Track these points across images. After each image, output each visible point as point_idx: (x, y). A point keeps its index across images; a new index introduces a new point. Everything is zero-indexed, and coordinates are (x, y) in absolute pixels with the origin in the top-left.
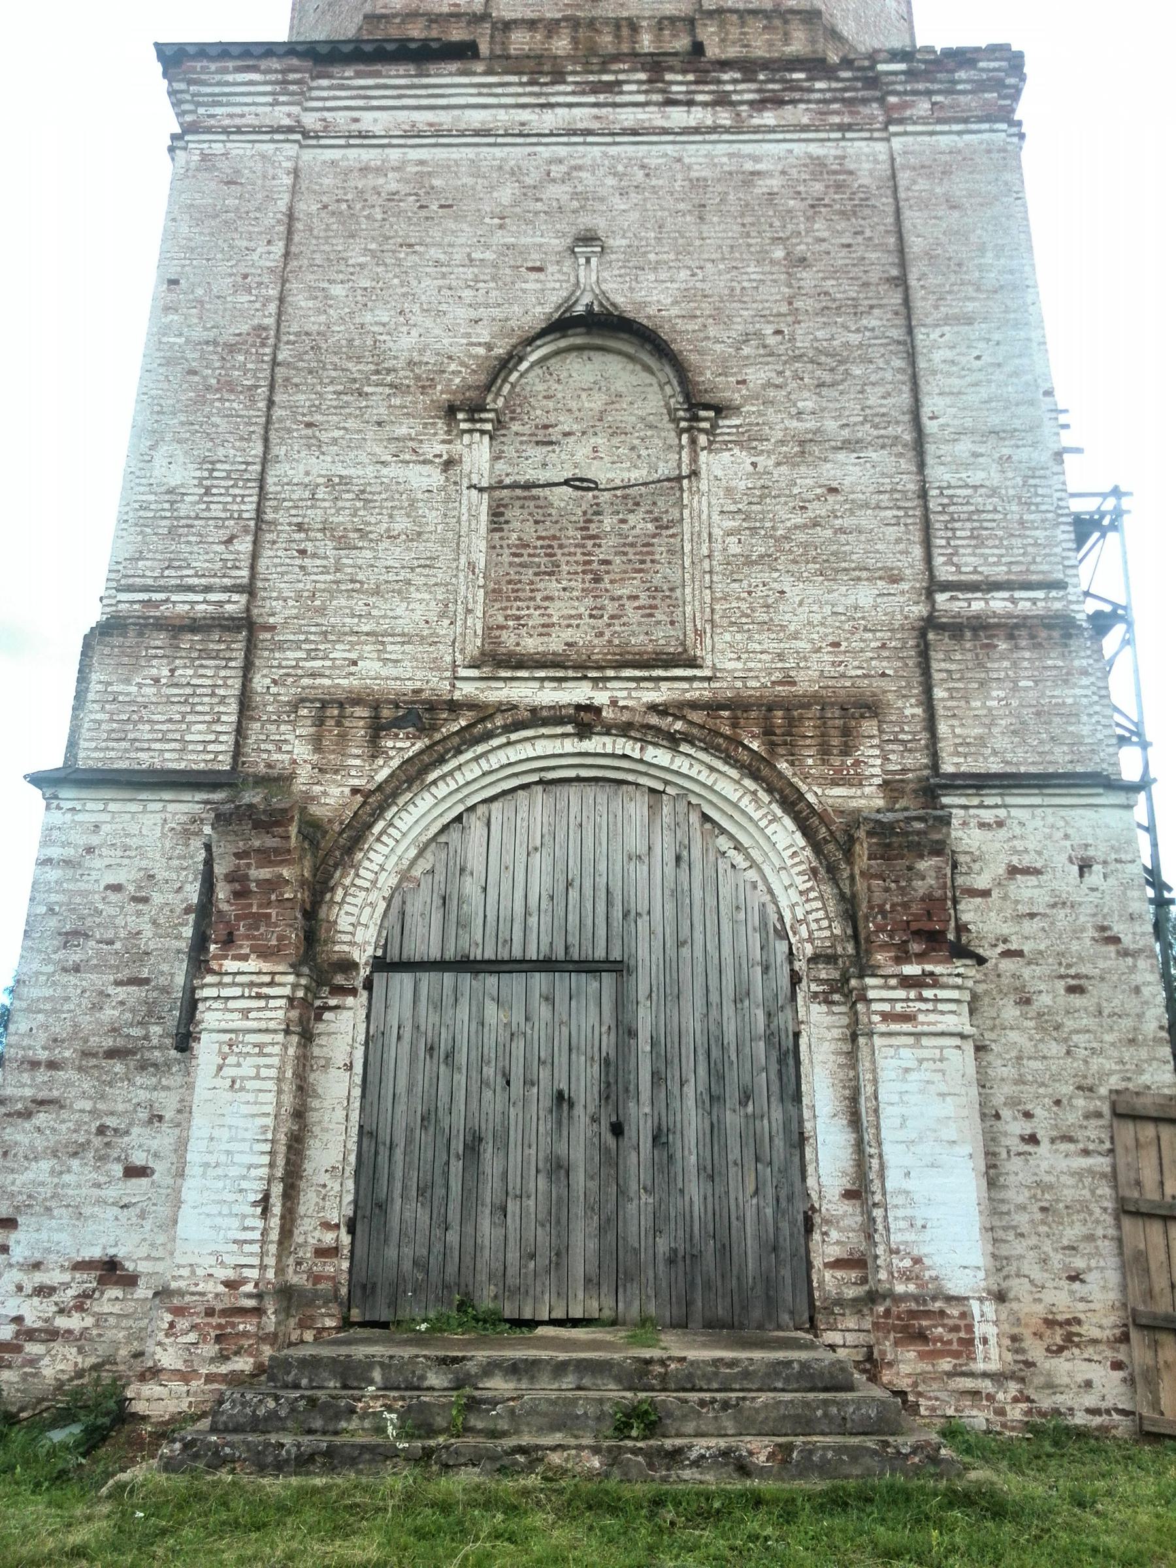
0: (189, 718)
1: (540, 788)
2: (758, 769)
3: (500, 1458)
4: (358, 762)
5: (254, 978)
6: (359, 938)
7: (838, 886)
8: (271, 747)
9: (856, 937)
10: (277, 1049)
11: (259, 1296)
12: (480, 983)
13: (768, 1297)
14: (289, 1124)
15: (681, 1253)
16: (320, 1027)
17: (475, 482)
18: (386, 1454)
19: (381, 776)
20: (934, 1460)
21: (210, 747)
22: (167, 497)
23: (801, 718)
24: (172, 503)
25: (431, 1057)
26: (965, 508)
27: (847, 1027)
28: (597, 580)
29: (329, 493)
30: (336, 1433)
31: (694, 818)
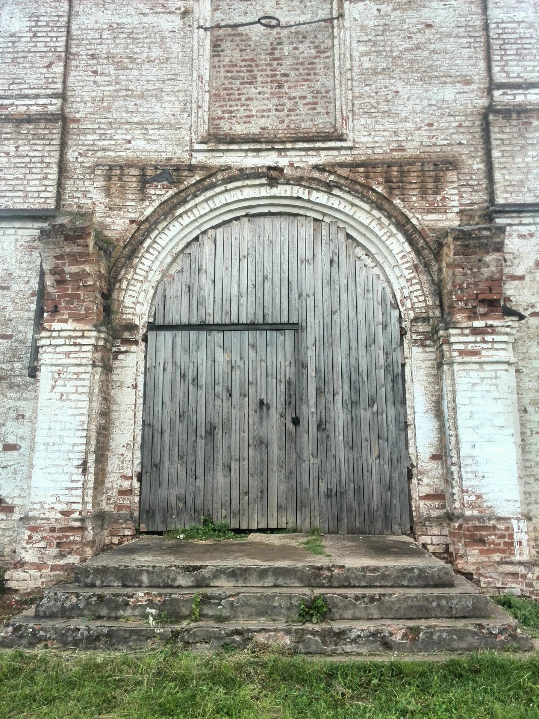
0: (29, 177)
1: (246, 219)
2: (382, 204)
3: (223, 638)
4: (133, 203)
5: (71, 333)
6: (138, 311)
7: (431, 275)
8: (79, 195)
9: (441, 306)
10: (88, 376)
11: (82, 520)
12: (212, 337)
13: (386, 516)
14: (98, 419)
15: (334, 492)
16: (117, 363)
17: (202, 23)
18: (149, 635)
19: (148, 212)
20: (514, 637)
21: (42, 195)
22: (10, 39)
23: (409, 171)
24: (13, 43)
25: (184, 380)
26: (513, 36)
27: (435, 360)
28: (280, 87)
29: (111, 34)
30: (117, 618)
31: (342, 236)
